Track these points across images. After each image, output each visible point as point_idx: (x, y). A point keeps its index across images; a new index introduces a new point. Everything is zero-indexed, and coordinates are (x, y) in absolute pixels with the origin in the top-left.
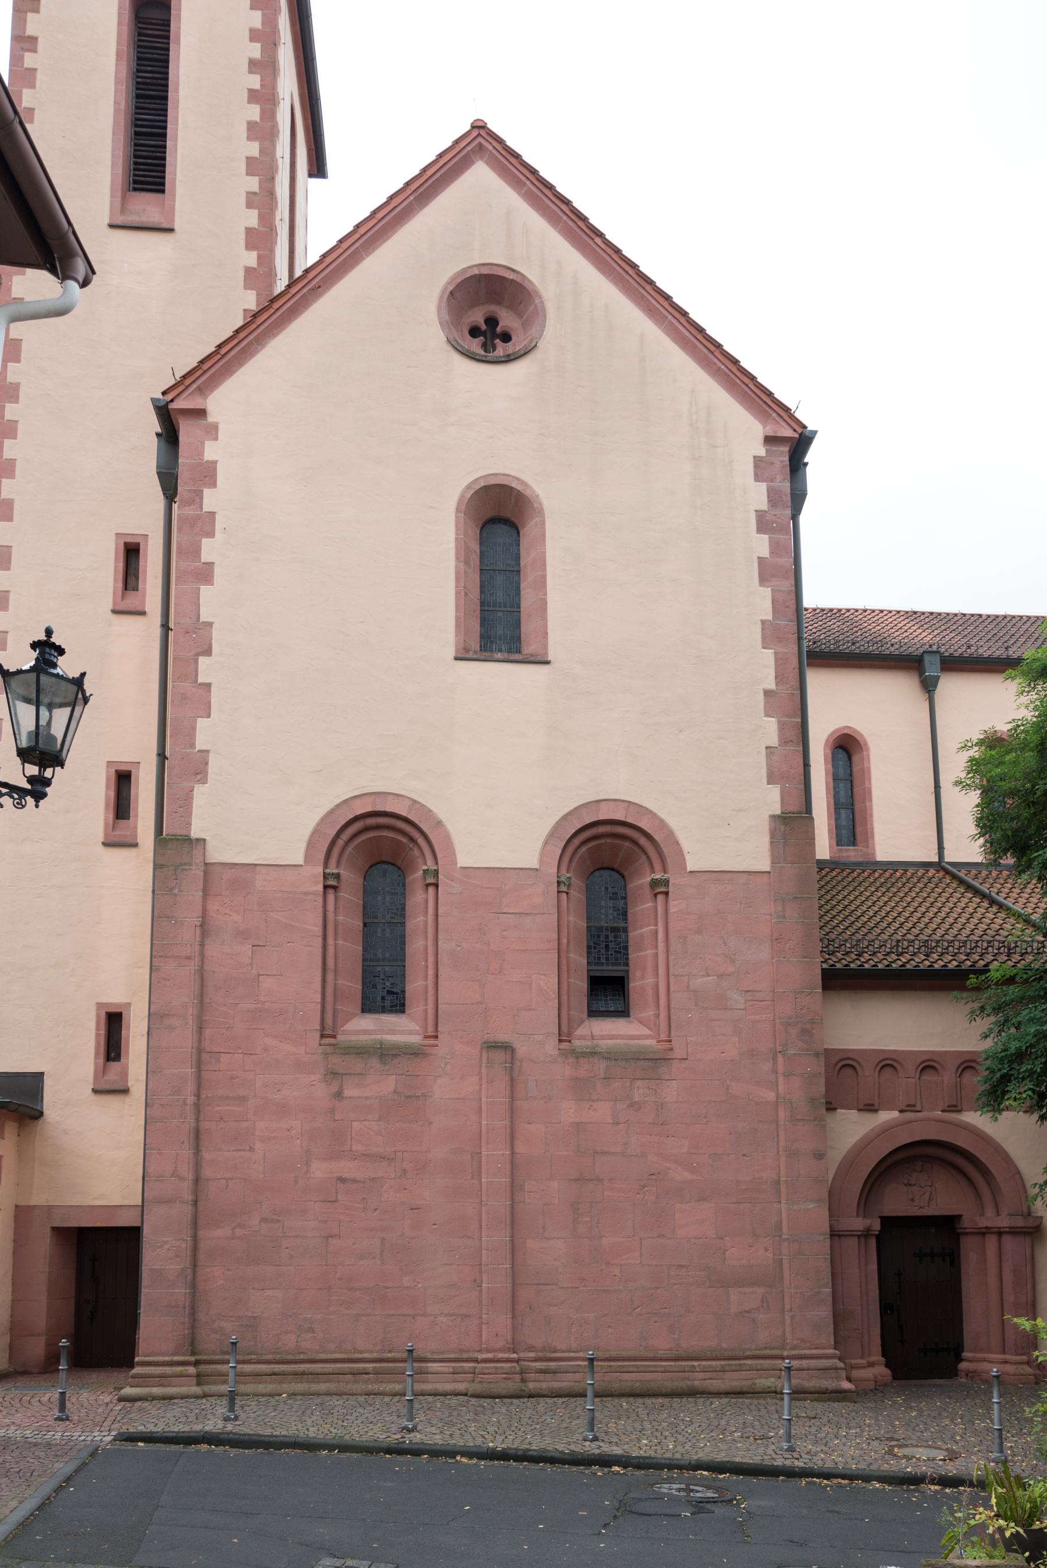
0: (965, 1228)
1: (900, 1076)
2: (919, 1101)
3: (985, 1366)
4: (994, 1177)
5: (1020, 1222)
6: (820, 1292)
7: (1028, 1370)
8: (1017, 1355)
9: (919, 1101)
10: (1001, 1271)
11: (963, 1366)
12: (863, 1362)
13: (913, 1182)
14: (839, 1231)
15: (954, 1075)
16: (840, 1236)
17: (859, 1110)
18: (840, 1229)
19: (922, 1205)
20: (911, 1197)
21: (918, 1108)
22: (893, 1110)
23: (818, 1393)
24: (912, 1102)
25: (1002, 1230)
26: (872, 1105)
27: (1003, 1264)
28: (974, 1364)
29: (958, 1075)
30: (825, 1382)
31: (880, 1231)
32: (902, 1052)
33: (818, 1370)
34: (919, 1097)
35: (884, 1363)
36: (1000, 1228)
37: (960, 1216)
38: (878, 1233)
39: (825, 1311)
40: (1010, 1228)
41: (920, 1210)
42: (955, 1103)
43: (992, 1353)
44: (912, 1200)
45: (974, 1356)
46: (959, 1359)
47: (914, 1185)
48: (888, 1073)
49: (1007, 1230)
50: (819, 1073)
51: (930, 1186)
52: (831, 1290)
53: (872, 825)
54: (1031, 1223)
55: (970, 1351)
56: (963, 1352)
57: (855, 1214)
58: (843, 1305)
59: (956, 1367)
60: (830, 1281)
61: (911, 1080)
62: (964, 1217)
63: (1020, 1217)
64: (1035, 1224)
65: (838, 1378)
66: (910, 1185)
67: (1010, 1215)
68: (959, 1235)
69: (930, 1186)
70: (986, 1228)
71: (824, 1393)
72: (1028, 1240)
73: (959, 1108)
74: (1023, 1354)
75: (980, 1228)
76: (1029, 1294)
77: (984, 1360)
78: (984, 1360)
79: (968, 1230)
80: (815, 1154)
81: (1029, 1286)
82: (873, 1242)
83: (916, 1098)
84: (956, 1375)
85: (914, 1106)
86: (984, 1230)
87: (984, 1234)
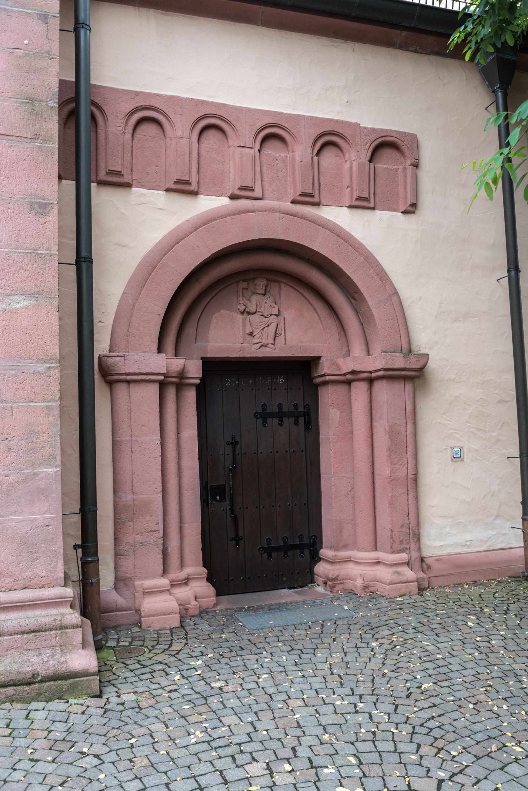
0: (324, 375)
1: (231, 142)
2: (258, 183)
3: (351, 569)
4: (363, 299)
5: (399, 362)
6: (35, 474)
7: (409, 574)
8: (393, 552)
9: (258, 183)
10: (372, 434)
11: (321, 568)
12: (164, 582)
14: (127, 374)
15: (309, 151)
16: (128, 382)
17: (168, 190)
18: (128, 371)
19: (264, 342)
20: (249, 330)
21: (258, 193)
22: (221, 195)
23: (15, 685)
24: (248, 183)
25: (374, 375)
26: (187, 183)
27: (374, 424)
28: (336, 567)
29: (315, 152)
30: (35, 660)
32: (235, 108)
33: (23, 633)
34: (258, 177)
35: (205, 576)
36: (370, 372)
37: (317, 359)
38: (198, 381)
40: (385, 370)
42: (310, 191)
43: (359, 550)
44: (251, 334)
45: (335, 556)
46: (315, 558)
47: (254, 313)
48: (212, 136)
49: (381, 373)
50: (48, 52)
51: (277, 316)
52: (59, 469)
54: (414, 364)
55: (331, 548)
57: (155, 348)
60: (58, 452)
61: (249, 150)
62: (323, 360)
63: (398, 354)
64: (419, 366)
65: (64, 647)
66: (249, 313)
67: (383, 351)
68: (316, 387)
69: (277, 316)
70: (353, 372)
71: (29, 684)
72: (409, 387)
73: (316, 199)
74: (401, 551)
75: (345, 375)
76: (409, 465)
77: (349, 560)
78: (349, 560)
79: (327, 378)
80: (32, 204)
81: (410, 454)
83: (254, 179)
84: (312, 581)
85: (251, 189)
86: (349, 377)
87: (349, 383)
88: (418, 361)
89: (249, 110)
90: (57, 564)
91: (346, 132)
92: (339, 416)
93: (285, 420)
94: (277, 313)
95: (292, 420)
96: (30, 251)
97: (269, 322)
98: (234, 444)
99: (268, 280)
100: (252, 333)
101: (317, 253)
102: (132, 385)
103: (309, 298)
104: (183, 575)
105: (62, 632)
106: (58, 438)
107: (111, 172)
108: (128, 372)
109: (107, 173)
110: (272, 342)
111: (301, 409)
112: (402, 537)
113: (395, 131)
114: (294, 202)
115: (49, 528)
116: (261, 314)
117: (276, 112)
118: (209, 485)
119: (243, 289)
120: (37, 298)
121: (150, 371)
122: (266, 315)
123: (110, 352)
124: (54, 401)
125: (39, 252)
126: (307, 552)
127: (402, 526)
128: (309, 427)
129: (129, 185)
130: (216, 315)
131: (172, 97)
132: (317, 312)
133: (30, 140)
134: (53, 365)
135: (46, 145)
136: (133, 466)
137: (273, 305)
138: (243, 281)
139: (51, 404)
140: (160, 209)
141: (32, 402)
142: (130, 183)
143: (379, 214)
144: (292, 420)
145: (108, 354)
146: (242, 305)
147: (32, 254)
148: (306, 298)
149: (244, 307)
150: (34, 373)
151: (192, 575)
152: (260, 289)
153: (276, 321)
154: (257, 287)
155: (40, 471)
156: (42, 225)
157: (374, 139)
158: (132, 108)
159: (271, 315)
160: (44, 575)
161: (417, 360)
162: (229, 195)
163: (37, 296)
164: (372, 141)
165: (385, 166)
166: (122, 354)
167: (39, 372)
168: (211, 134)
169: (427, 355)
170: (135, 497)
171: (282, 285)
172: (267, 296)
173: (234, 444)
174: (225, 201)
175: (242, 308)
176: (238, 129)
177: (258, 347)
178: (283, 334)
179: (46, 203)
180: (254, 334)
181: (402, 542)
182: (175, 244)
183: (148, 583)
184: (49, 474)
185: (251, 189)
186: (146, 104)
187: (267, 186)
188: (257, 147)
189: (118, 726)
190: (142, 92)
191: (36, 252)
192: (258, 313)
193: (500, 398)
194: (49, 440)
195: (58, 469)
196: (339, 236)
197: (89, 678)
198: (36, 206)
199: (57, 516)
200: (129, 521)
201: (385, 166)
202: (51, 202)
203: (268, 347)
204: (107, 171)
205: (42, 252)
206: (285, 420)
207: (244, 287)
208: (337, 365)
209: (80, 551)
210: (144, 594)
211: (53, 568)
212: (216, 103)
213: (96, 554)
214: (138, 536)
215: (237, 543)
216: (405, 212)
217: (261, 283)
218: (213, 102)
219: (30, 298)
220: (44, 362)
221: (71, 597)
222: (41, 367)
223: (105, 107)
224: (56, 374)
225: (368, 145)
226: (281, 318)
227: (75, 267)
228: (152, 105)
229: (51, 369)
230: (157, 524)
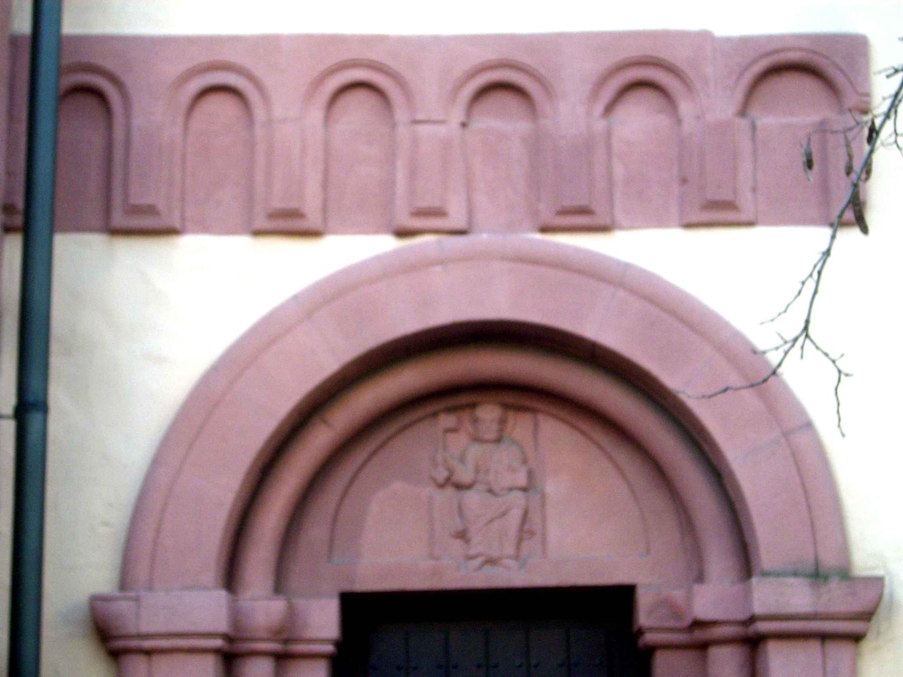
13: (464, 475)
16: (149, 653)
19: (495, 553)
21: (456, 220)
29: (599, 108)
31: (338, 644)
32: (404, 41)
38: (329, 648)
41: (487, 569)
51: (525, 490)
64: (856, 606)
85: (439, 213)
91: (678, 56)
129: (170, 232)
145: (117, 593)
146: (441, 468)
152: (489, 429)
165: (784, 120)
168: (359, 101)
171: (541, 417)
174: (387, 244)
175: (442, 475)
185: (439, 213)
187: (481, 199)
188: (457, 114)
192: (480, 487)
201: (784, 120)
223: (126, 79)
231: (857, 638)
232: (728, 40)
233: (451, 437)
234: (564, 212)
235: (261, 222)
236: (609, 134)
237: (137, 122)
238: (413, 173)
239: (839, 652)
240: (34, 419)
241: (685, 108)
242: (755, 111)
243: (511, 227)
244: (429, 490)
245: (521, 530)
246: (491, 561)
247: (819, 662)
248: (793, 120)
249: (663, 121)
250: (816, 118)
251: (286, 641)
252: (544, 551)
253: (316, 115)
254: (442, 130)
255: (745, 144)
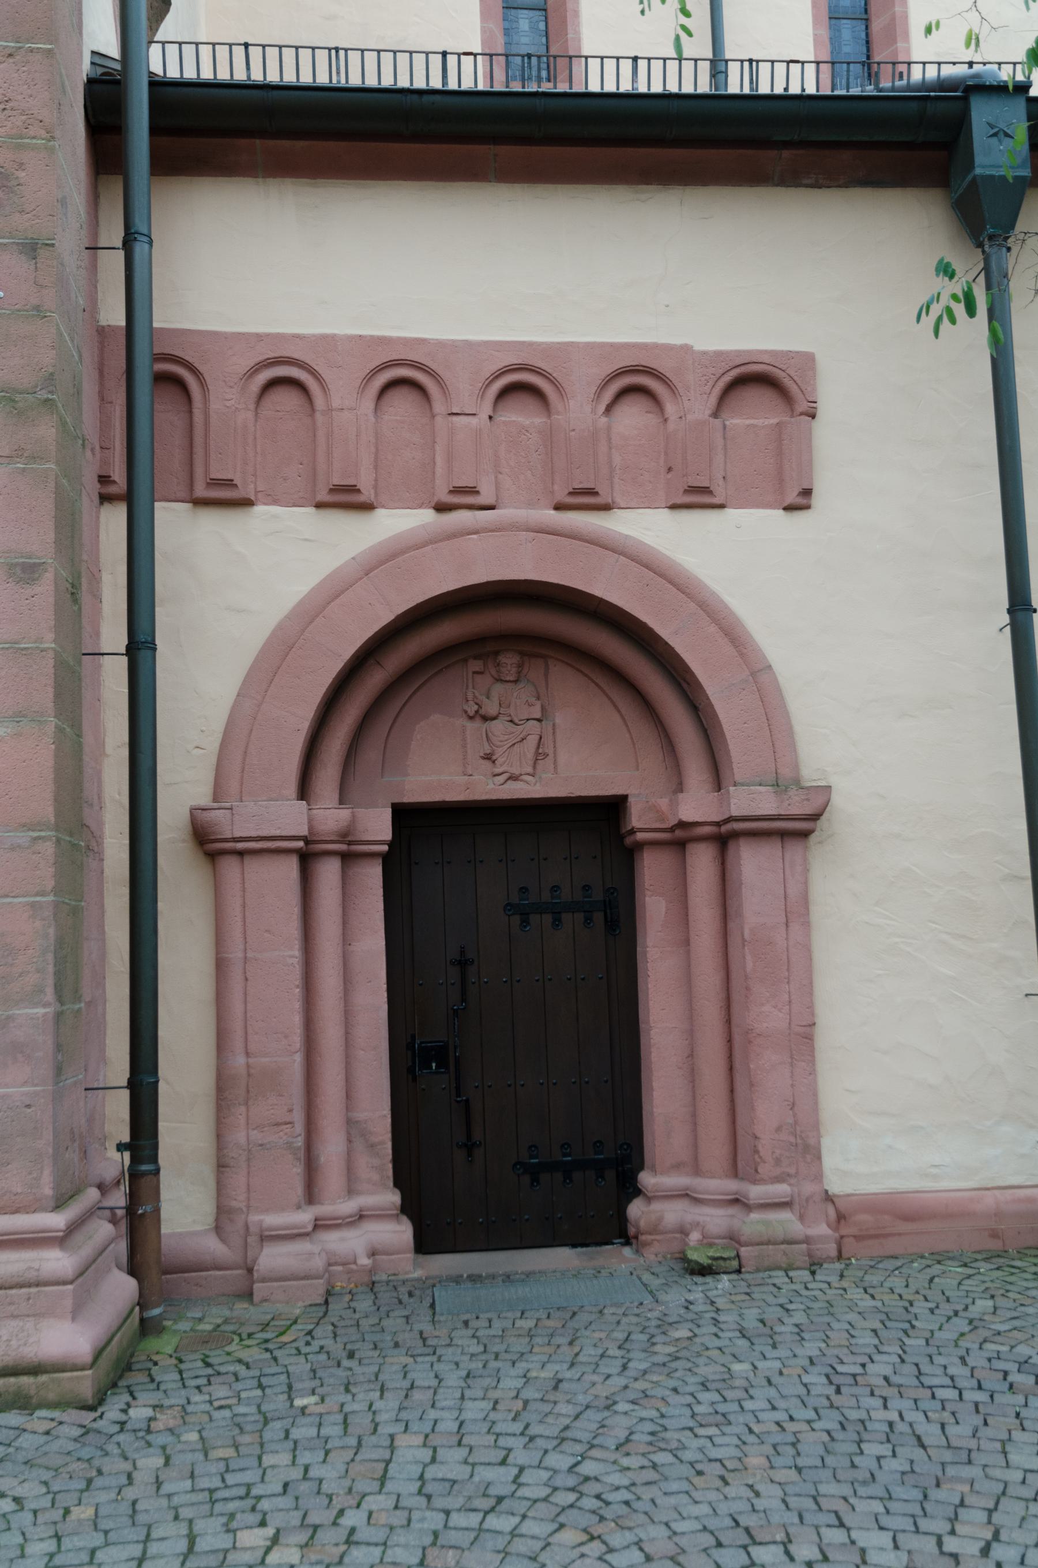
6: (10, 1018)
12: (304, 1217)
13: (491, 709)
16: (241, 854)
19: (516, 771)
26: (353, 489)
29: (602, 408)
31: (391, 844)
32: (441, 344)
38: (386, 848)
39: (25, 1083)
41: (511, 784)
47: (494, 718)
48: (402, 402)
51: (539, 720)
53: (578, 33)
56: (641, 1167)
58: (247, 1054)
59: (624, 1210)
60: (50, 981)
64: (808, 809)
66: (486, 719)
82: (373, 875)
85: (473, 491)
88: (808, 800)
89: (468, 343)
90: (42, 1172)
92: (664, 910)
93: (566, 917)
94: (538, 715)
95: (580, 917)
96: (7, 646)
97: (524, 733)
98: (463, 963)
99: (522, 654)
100: (491, 754)
101: (601, 601)
102: (247, 859)
103: (602, 684)
104: (348, 1207)
105: (39, 1292)
106: (50, 957)
107: (216, 483)
108: (238, 836)
109: (208, 484)
110: (530, 770)
111: (598, 895)
112: (778, 1152)
113: (766, 352)
114: (558, 507)
115: (29, 1110)
116: (509, 718)
117: (523, 343)
118: (418, 1042)
119: (474, 673)
120: (18, 722)
121: (278, 833)
122: (517, 721)
123: (215, 800)
124: (42, 893)
125: (22, 646)
126: (610, 1175)
127: (779, 1129)
128: (615, 930)
129: (246, 503)
130: (422, 723)
131: (324, 337)
132: (619, 711)
133: (7, 460)
134: (43, 834)
135: (34, 466)
136: (248, 1005)
137: (533, 700)
138: (476, 658)
139: (38, 899)
140: (306, 540)
141: (7, 896)
142: (249, 499)
143: (732, 515)
144: (580, 917)
146: (471, 703)
147: (11, 650)
148: (597, 685)
149: (476, 707)
150: (12, 848)
151: (368, 1210)
153: (538, 731)
154: (503, 670)
155: (18, 1012)
156: (28, 601)
157: (721, 371)
158: (252, 365)
159: (528, 720)
160: (19, 1190)
161: (804, 800)
162: (433, 505)
163: (18, 719)
164: (718, 376)
166: (228, 805)
167: (19, 846)
169: (828, 788)
170: (251, 1060)
172: (521, 685)
173: (463, 963)
174: (424, 517)
175: (472, 709)
176: (448, 383)
177: (502, 781)
178: (551, 755)
179: (34, 564)
180: (494, 758)
181: (778, 1162)
182: (329, 603)
183: (273, 1220)
184: (32, 1018)
186: (276, 355)
188: (487, 408)
189: (88, 1457)
190: (268, 335)
191: (17, 646)
193: (1007, 871)
194: (35, 960)
195: (48, 1010)
196: (647, 566)
197: (75, 1374)
198: (18, 571)
199: (44, 1090)
200: (239, 1104)
202: (43, 561)
203: (522, 780)
204: (208, 481)
205: (26, 646)
206: (566, 917)
207: (477, 669)
208: (657, 811)
209: (127, 1155)
210: (262, 1240)
211: (35, 1179)
212: (405, 338)
213: (154, 1159)
214: (255, 1132)
215: (470, 1154)
216: (789, 508)
217: (509, 661)
218: (399, 338)
219: (6, 724)
220: (29, 830)
221: (61, 1231)
222: (23, 838)
224: (48, 849)
225: (710, 384)
226: (547, 725)
227: (125, 659)
228: (287, 355)
229: (40, 841)
230: (290, 1111)
231: (805, 834)
232: (704, 353)
233: (478, 678)
234: (574, 493)
235: (323, 496)
236: (609, 428)
237: (215, 405)
238: (450, 458)
239: (794, 849)
240: (143, 655)
241: (670, 408)
242: (724, 415)
243: (531, 504)
244: (461, 721)
245: (537, 753)
246: (513, 778)
247: (781, 854)
248: (759, 422)
249: (652, 419)
250: (774, 421)
251: (350, 843)
252: (555, 768)
253: (368, 403)
254: (474, 421)
255: (719, 442)
